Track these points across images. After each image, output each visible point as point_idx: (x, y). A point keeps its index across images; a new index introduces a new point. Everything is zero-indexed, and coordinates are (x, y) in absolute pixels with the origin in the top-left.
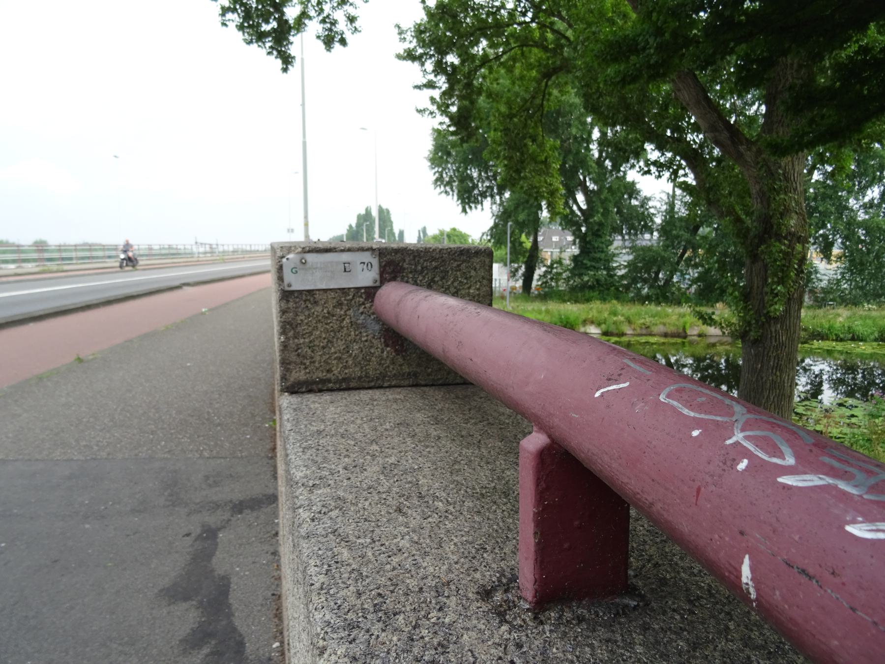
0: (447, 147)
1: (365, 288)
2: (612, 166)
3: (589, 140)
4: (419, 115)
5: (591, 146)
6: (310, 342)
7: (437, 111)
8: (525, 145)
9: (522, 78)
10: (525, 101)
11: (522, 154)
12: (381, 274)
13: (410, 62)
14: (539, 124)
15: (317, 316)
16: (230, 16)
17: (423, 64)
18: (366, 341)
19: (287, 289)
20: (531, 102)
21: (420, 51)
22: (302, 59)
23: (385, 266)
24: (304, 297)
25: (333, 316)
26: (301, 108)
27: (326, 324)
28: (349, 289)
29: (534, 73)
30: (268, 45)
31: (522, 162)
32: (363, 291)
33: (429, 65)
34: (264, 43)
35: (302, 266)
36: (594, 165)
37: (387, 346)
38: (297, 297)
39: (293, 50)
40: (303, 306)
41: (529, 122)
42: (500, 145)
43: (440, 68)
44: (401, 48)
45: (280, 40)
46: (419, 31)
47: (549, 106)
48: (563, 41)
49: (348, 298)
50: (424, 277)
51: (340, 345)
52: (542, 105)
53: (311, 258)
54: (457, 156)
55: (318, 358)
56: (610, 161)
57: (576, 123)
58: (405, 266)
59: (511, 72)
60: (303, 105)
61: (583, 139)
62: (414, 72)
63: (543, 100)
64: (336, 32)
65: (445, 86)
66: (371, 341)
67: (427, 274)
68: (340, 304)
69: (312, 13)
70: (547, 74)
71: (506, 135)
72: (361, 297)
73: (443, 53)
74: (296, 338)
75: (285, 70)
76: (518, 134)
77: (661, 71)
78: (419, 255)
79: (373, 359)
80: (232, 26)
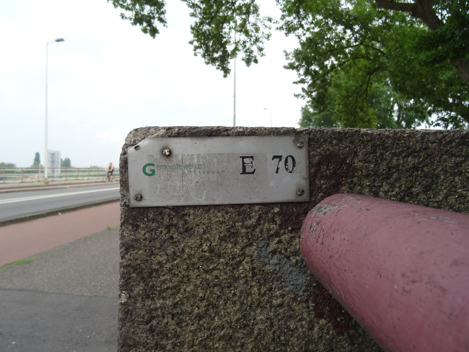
0: (309, 117)
1: (281, 204)
2: (406, 125)
3: (392, 111)
4: (296, 98)
5: (393, 114)
6: (175, 305)
7: (306, 95)
8: (357, 112)
9: (354, 76)
10: (357, 88)
11: (355, 117)
12: (312, 178)
13: (291, 70)
14: (365, 101)
15: (190, 256)
16: (198, 50)
17: (298, 71)
18: (281, 306)
19: (134, 203)
20: (360, 89)
21: (297, 64)
22: (235, 73)
23: (319, 163)
24: (166, 221)
25: (219, 256)
26: (233, 98)
27: (206, 272)
28: (251, 205)
29: (360, 73)
30: (217, 64)
31: (355, 122)
32: (276, 210)
33: (302, 71)
34: (215, 63)
35: (163, 162)
36: (395, 124)
37: (320, 315)
38: (153, 220)
39: (230, 66)
40: (164, 236)
41: (359, 99)
42: (342, 112)
43: (307, 73)
44: (286, 63)
45: (223, 62)
46: (297, 54)
47: (371, 90)
48: (379, 54)
49: (249, 223)
50: (392, 186)
51: (231, 312)
52: (366, 90)
53: (180, 146)
54: (315, 121)
55: (189, 337)
56: (405, 122)
57: (384, 101)
58: (358, 164)
59: (348, 73)
60: (235, 96)
61: (388, 110)
62: (294, 75)
63: (367, 87)
64: (252, 57)
65: (310, 82)
66: (289, 306)
67: (398, 179)
68: (232, 235)
69: (240, 48)
70: (370, 73)
71: (345, 107)
72: (274, 222)
73: (309, 64)
74: (148, 297)
75: (225, 76)
76: (352, 106)
77: (461, 54)
78: (384, 143)
79: (293, 340)
80: (199, 55)
